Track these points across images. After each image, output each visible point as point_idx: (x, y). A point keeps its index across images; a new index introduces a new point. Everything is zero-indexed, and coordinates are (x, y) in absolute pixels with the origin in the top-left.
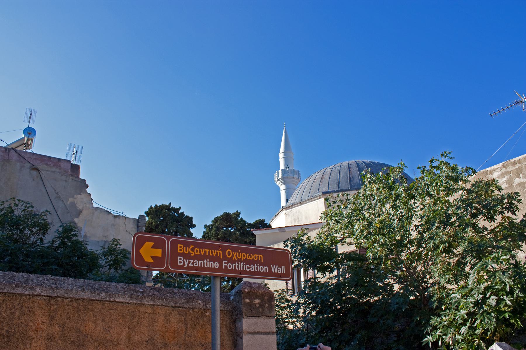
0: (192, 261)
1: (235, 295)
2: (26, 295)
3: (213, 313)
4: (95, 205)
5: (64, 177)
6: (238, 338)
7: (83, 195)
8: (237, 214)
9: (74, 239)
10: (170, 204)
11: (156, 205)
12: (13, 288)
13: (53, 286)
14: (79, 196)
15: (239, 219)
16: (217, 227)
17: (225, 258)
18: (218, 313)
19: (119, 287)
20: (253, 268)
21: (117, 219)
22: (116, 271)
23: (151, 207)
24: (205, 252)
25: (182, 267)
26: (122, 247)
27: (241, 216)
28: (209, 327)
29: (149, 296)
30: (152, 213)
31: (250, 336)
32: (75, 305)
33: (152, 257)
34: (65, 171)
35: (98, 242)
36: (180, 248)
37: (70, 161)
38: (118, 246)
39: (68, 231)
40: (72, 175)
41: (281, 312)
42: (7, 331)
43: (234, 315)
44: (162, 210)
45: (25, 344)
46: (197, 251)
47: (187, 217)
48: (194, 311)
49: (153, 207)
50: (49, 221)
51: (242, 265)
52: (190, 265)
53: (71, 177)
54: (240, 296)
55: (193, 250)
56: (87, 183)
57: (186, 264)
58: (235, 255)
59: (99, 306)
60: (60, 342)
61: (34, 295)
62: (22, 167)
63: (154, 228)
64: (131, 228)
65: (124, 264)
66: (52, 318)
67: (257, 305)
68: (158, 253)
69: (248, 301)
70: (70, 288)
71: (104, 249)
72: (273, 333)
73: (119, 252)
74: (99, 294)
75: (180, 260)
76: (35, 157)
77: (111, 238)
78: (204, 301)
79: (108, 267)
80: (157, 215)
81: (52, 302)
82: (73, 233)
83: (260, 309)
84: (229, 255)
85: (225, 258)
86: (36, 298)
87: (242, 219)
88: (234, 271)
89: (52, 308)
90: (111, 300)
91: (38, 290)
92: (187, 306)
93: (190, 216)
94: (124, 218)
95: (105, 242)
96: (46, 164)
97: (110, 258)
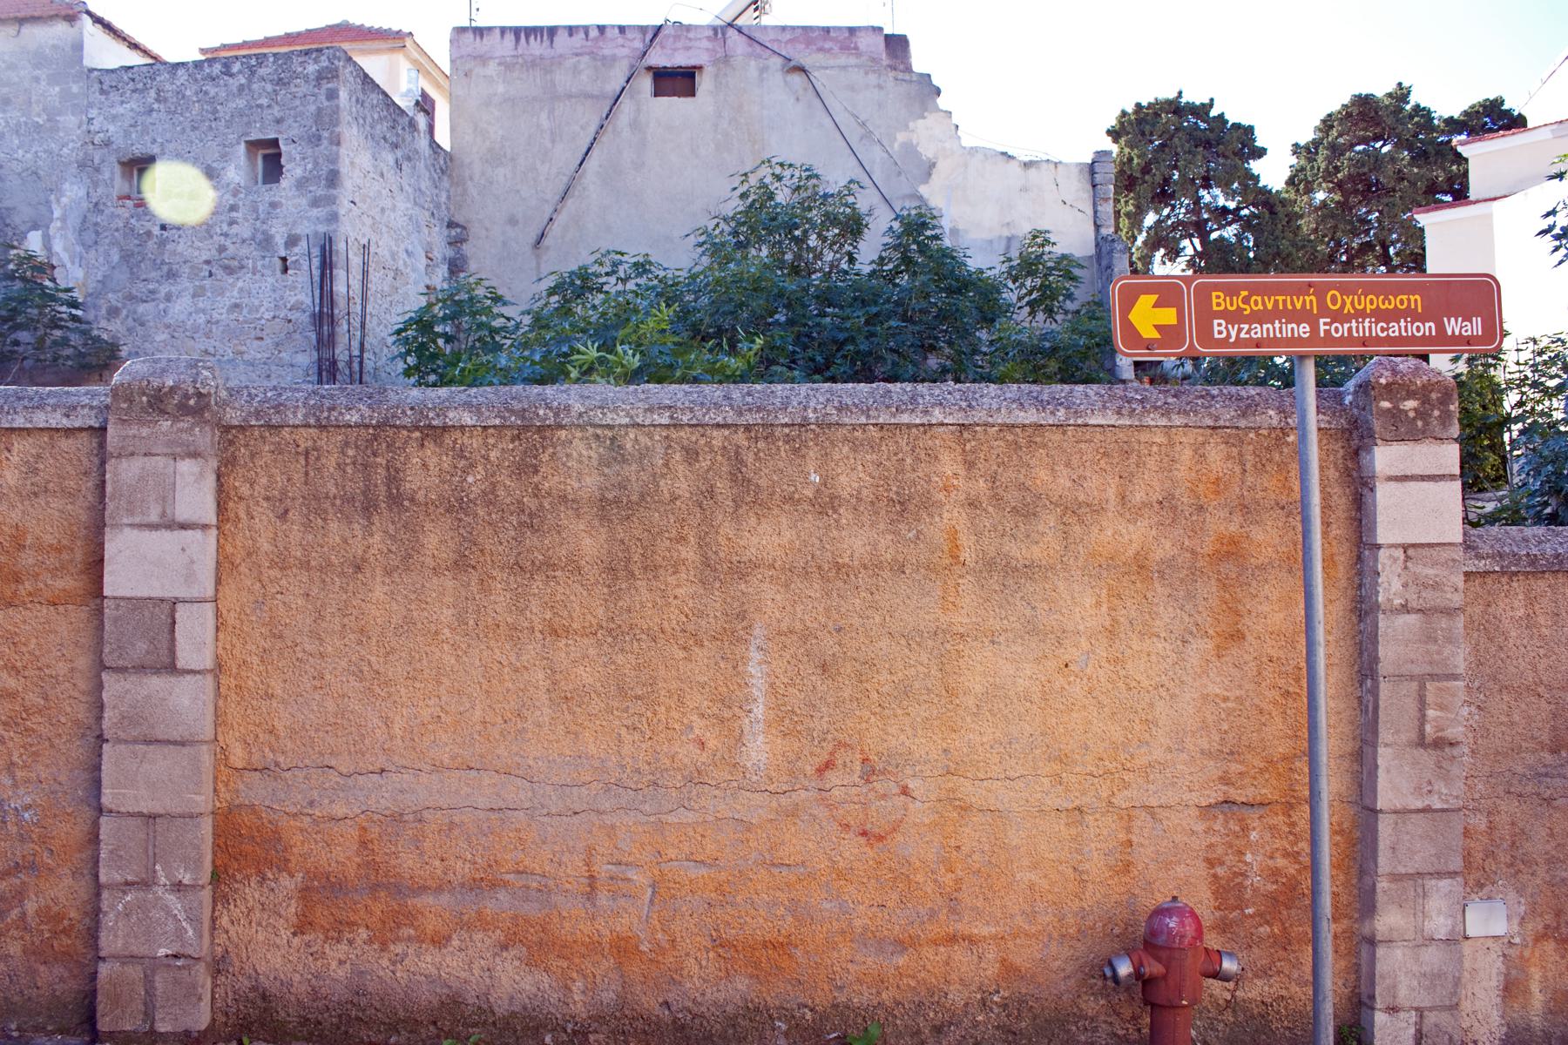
0: (1246, 327)
1: (1356, 392)
2: (917, 426)
3: (1303, 438)
4: (967, 142)
5: (872, 78)
6: (1365, 491)
7: (931, 119)
8: (1402, 94)
9: (934, 245)
10: (1180, 93)
11: (1138, 105)
12: (894, 416)
13: (964, 404)
14: (920, 121)
15: (1408, 107)
16: (1333, 147)
17: (1323, 311)
18: (1313, 436)
19: (1091, 393)
20: (1395, 330)
21: (1032, 171)
22: (1050, 316)
23: (1124, 114)
24: (1276, 302)
25: (1224, 342)
26: (1059, 250)
27: (1414, 99)
28: (1294, 466)
29: (1156, 408)
30: (1129, 128)
31: (1393, 484)
32: (1010, 437)
33: (1157, 327)
34: (873, 60)
35: (991, 242)
36: (1218, 301)
37: (881, 29)
38: (1047, 249)
39: (917, 228)
40: (894, 68)
41: (1547, 403)
42: (897, 493)
43: (1353, 440)
44: (1157, 115)
45: (931, 515)
46: (1256, 303)
47: (1237, 126)
48: (1258, 435)
49: (1130, 110)
50: (862, 206)
51: (1367, 324)
52: (1243, 335)
53: (892, 74)
54: (1366, 393)
55: (1246, 301)
56: (935, 81)
57: (1233, 334)
58: (1348, 302)
59: (1056, 437)
60: (990, 509)
61: (931, 425)
62: (763, 70)
63: (1138, 175)
64: (1077, 191)
65: (1070, 296)
66: (970, 465)
67: (1412, 414)
68: (1169, 316)
69: (1386, 404)
70: (995, 406)
71: (1010, 260)
72: (1452, 477)
73: (1050, 264)
74: (1052, 413)
75: (1219, 328)
76: (788, 36)
77: (1025, 229)
78: (1281, 410)
79: (1027, 309)
80: (1143, 134)
81: (966, 435)
82: (929, 233)
83: (1420, 423)
84: (1334, 303)
85: (1323, 311)
86: (935, 429)
87: (1417, 108)
88: (1349, 340)
89: (968, 447)
90: (1080, 421)
91: (937, 415)
92: (1242, 423)
93: (1245, 122)
94: (1052, 166)
95: (1009, 239)
96: (821, 49)
97: (1028, 283)
